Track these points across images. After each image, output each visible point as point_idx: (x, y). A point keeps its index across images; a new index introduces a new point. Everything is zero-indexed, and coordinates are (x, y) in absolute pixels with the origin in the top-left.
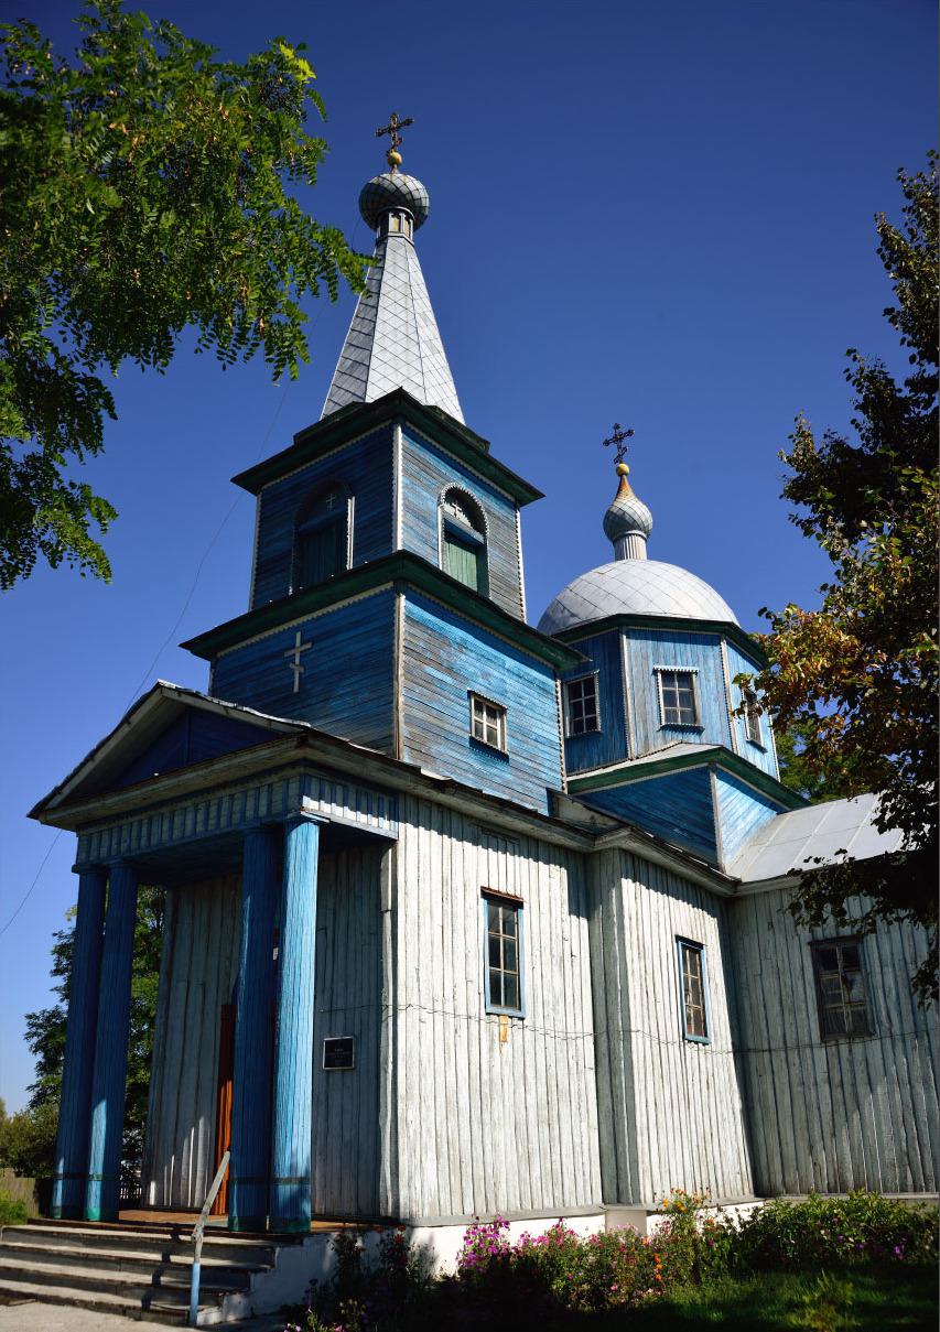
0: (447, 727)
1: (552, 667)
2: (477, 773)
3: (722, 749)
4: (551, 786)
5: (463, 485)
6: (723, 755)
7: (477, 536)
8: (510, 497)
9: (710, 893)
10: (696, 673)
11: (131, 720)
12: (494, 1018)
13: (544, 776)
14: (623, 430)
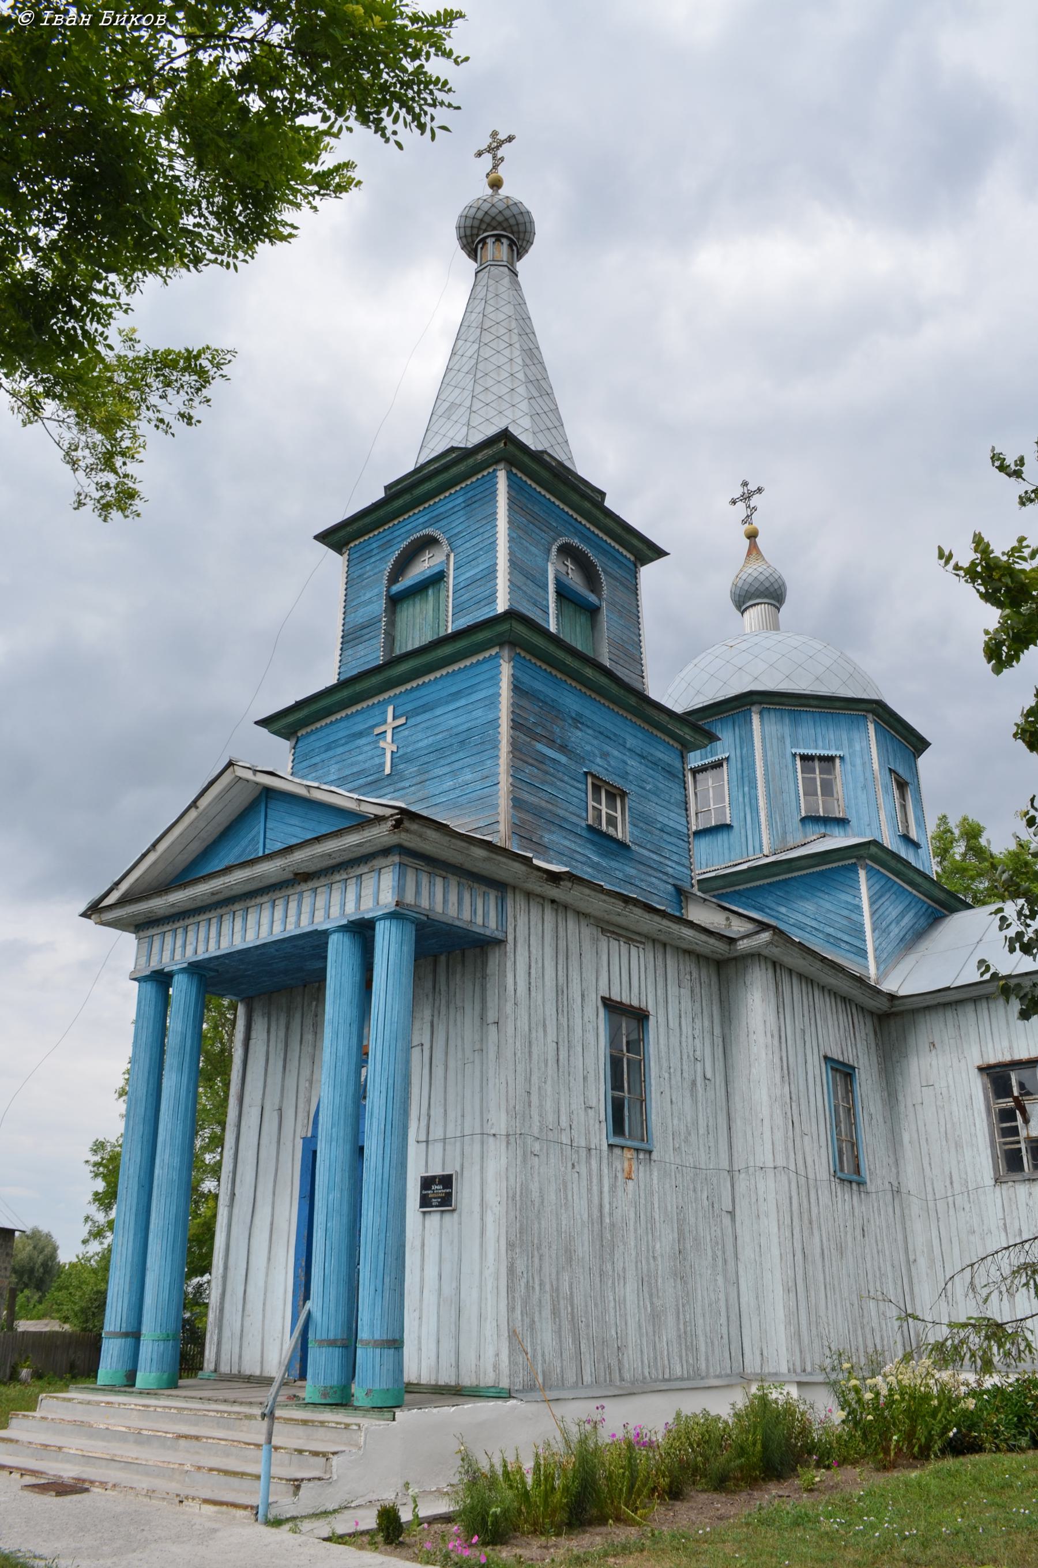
0: (562, 813)
1: (679, 747)
2: (595, 866)
3: (874, 843)
4: (679, 883)
5: (576, 542)
6: (873, 849)
7: (592, 598)
8: (629, 555)
9: (862, 1008)
10: (841, 758)
11: (199, 803)
12: (617, 1151)
13: (670, 871)
14: (752, 487)
